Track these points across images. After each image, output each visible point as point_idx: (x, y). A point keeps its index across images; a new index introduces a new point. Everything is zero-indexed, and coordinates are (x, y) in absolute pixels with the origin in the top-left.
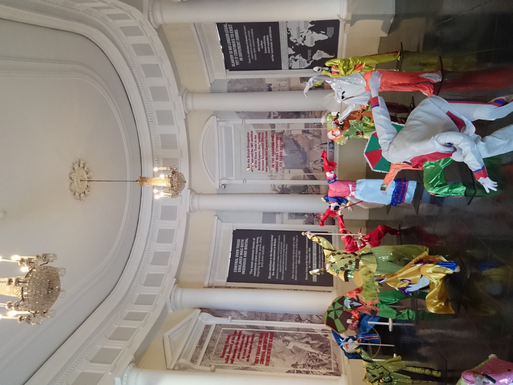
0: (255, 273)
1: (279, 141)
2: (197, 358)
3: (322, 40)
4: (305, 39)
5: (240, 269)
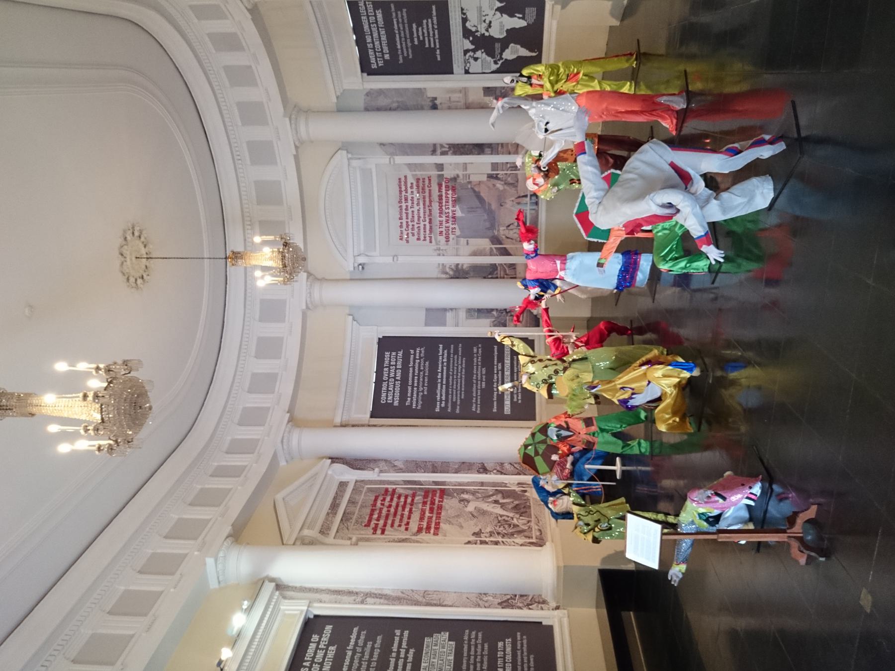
0: (414, 403)
1: (450, 192)
2: (329, 529)
3: (517, 27)
4: (490, 26)
5: (390, 398)
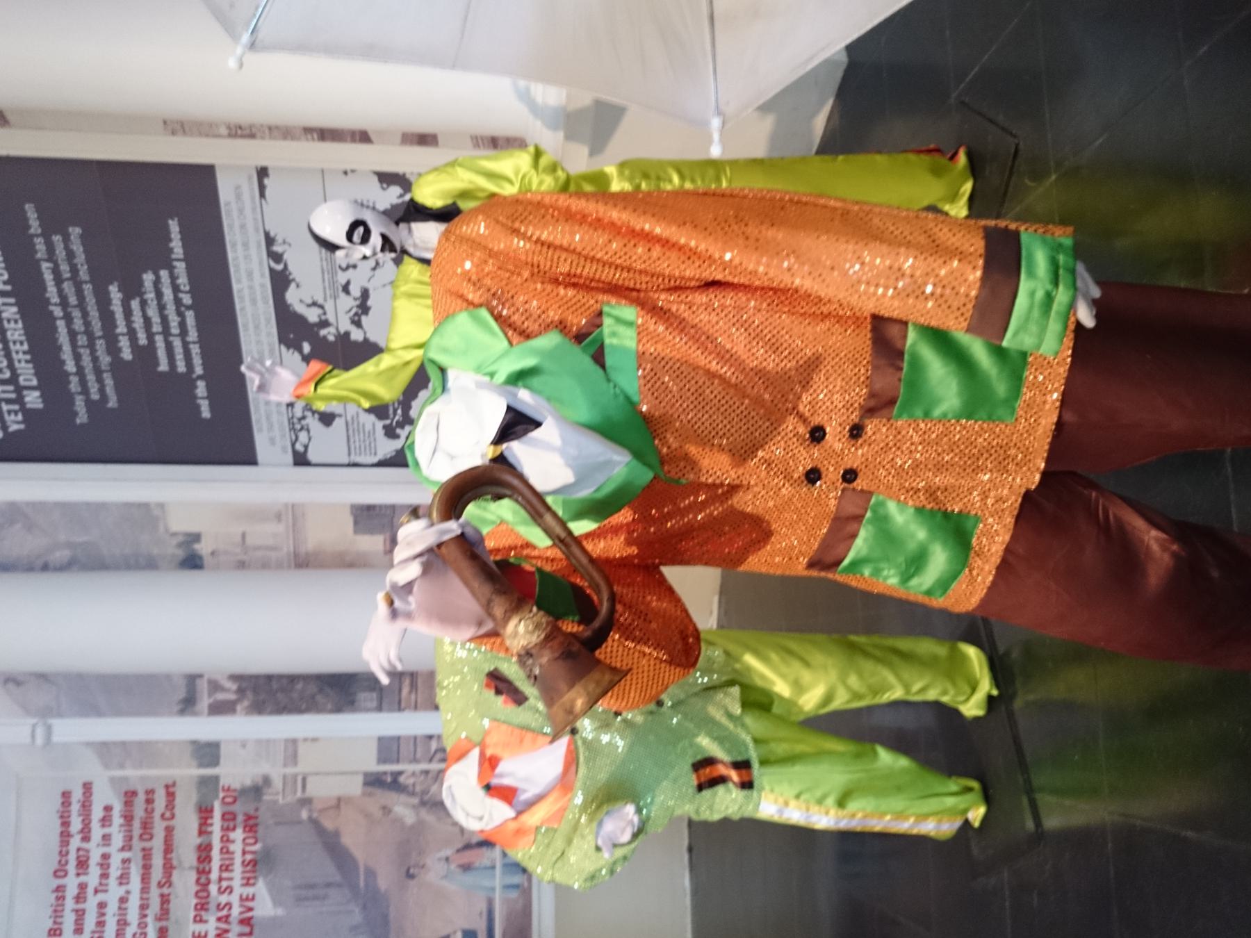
1: (238, 835)
4: (364, 308)
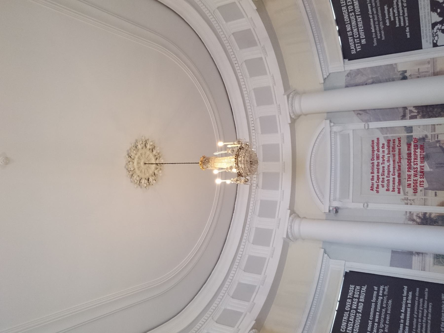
1: (419, 150)
